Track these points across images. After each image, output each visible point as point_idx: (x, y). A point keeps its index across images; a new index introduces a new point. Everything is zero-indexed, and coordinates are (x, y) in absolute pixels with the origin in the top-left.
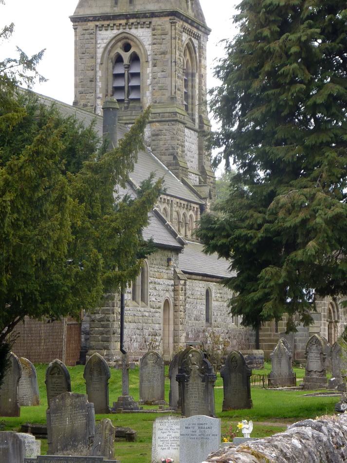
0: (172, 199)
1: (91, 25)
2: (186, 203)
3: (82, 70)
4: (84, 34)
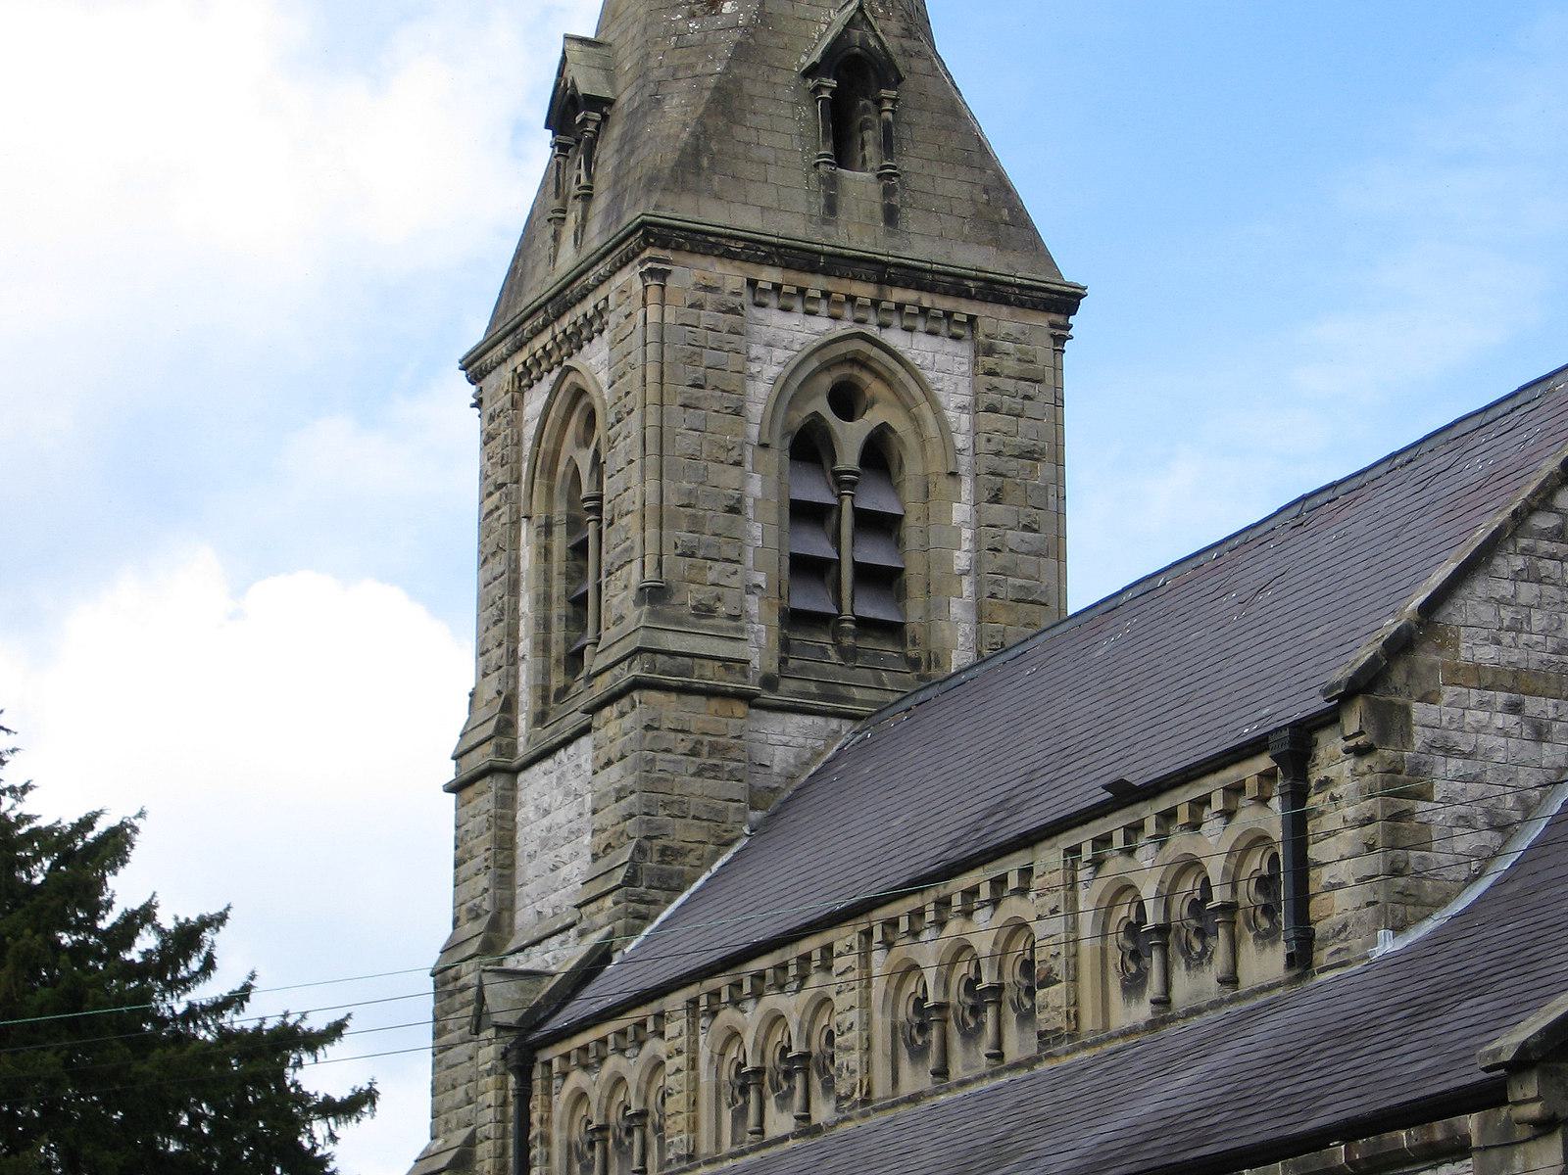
4: (701, 307)
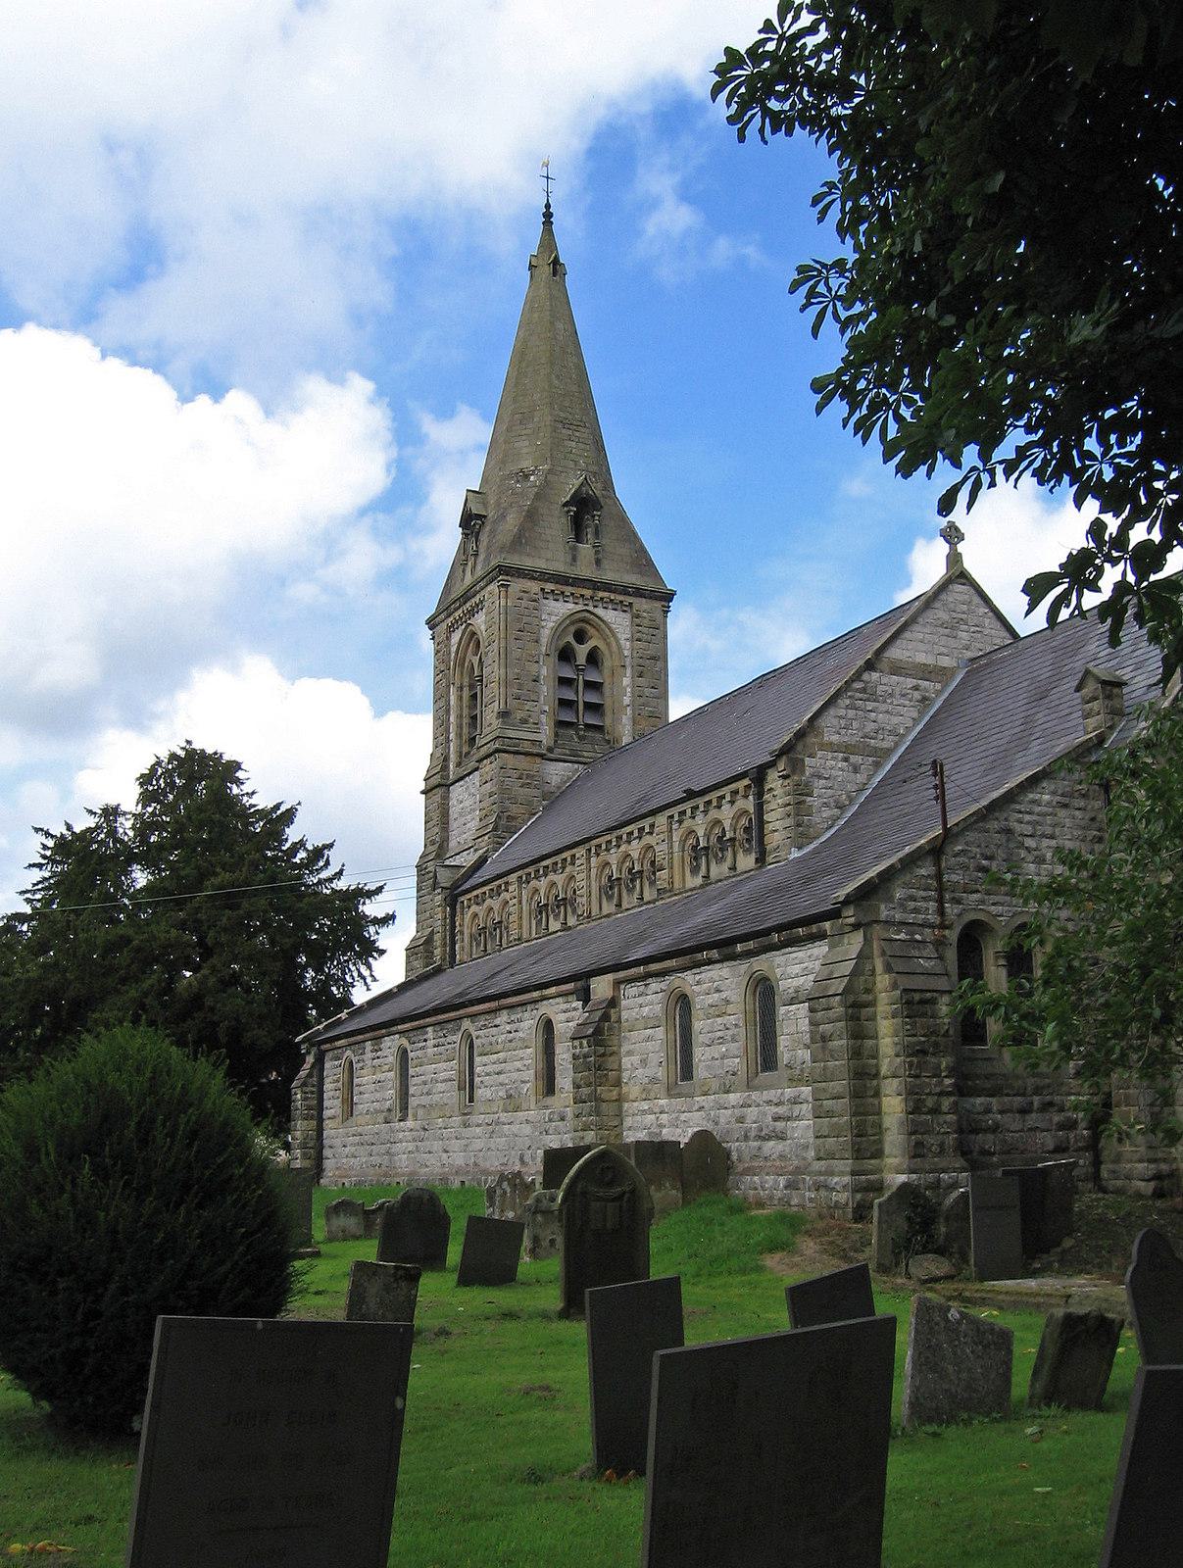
1: (534, 587)
3: (518, 660)
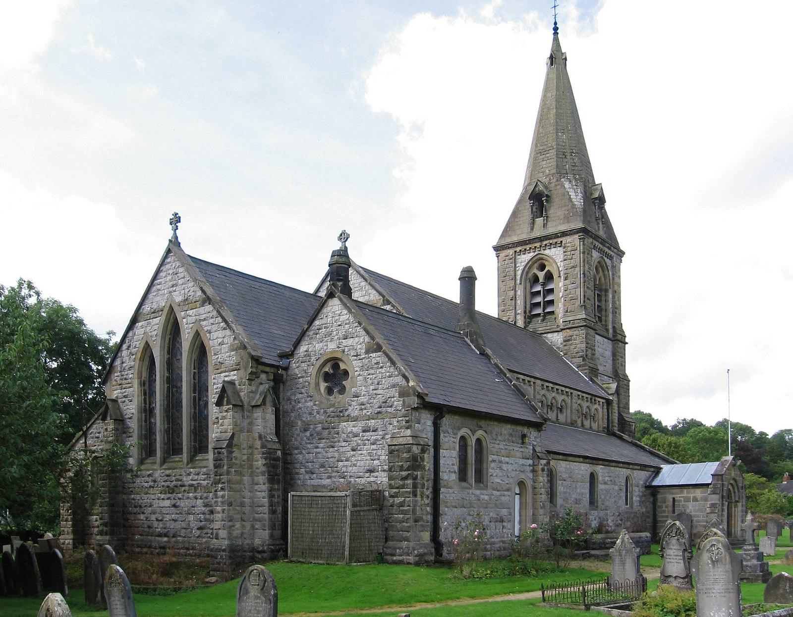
0: (572, 391)
1: (511, 252)
2: (589, 397)
